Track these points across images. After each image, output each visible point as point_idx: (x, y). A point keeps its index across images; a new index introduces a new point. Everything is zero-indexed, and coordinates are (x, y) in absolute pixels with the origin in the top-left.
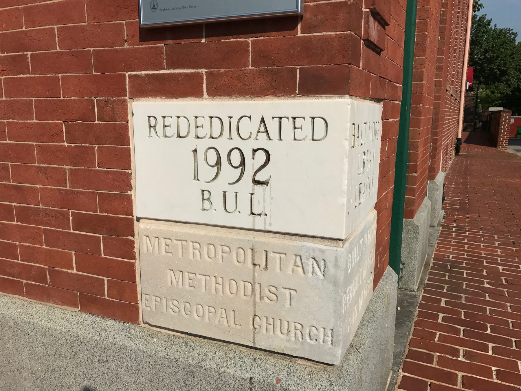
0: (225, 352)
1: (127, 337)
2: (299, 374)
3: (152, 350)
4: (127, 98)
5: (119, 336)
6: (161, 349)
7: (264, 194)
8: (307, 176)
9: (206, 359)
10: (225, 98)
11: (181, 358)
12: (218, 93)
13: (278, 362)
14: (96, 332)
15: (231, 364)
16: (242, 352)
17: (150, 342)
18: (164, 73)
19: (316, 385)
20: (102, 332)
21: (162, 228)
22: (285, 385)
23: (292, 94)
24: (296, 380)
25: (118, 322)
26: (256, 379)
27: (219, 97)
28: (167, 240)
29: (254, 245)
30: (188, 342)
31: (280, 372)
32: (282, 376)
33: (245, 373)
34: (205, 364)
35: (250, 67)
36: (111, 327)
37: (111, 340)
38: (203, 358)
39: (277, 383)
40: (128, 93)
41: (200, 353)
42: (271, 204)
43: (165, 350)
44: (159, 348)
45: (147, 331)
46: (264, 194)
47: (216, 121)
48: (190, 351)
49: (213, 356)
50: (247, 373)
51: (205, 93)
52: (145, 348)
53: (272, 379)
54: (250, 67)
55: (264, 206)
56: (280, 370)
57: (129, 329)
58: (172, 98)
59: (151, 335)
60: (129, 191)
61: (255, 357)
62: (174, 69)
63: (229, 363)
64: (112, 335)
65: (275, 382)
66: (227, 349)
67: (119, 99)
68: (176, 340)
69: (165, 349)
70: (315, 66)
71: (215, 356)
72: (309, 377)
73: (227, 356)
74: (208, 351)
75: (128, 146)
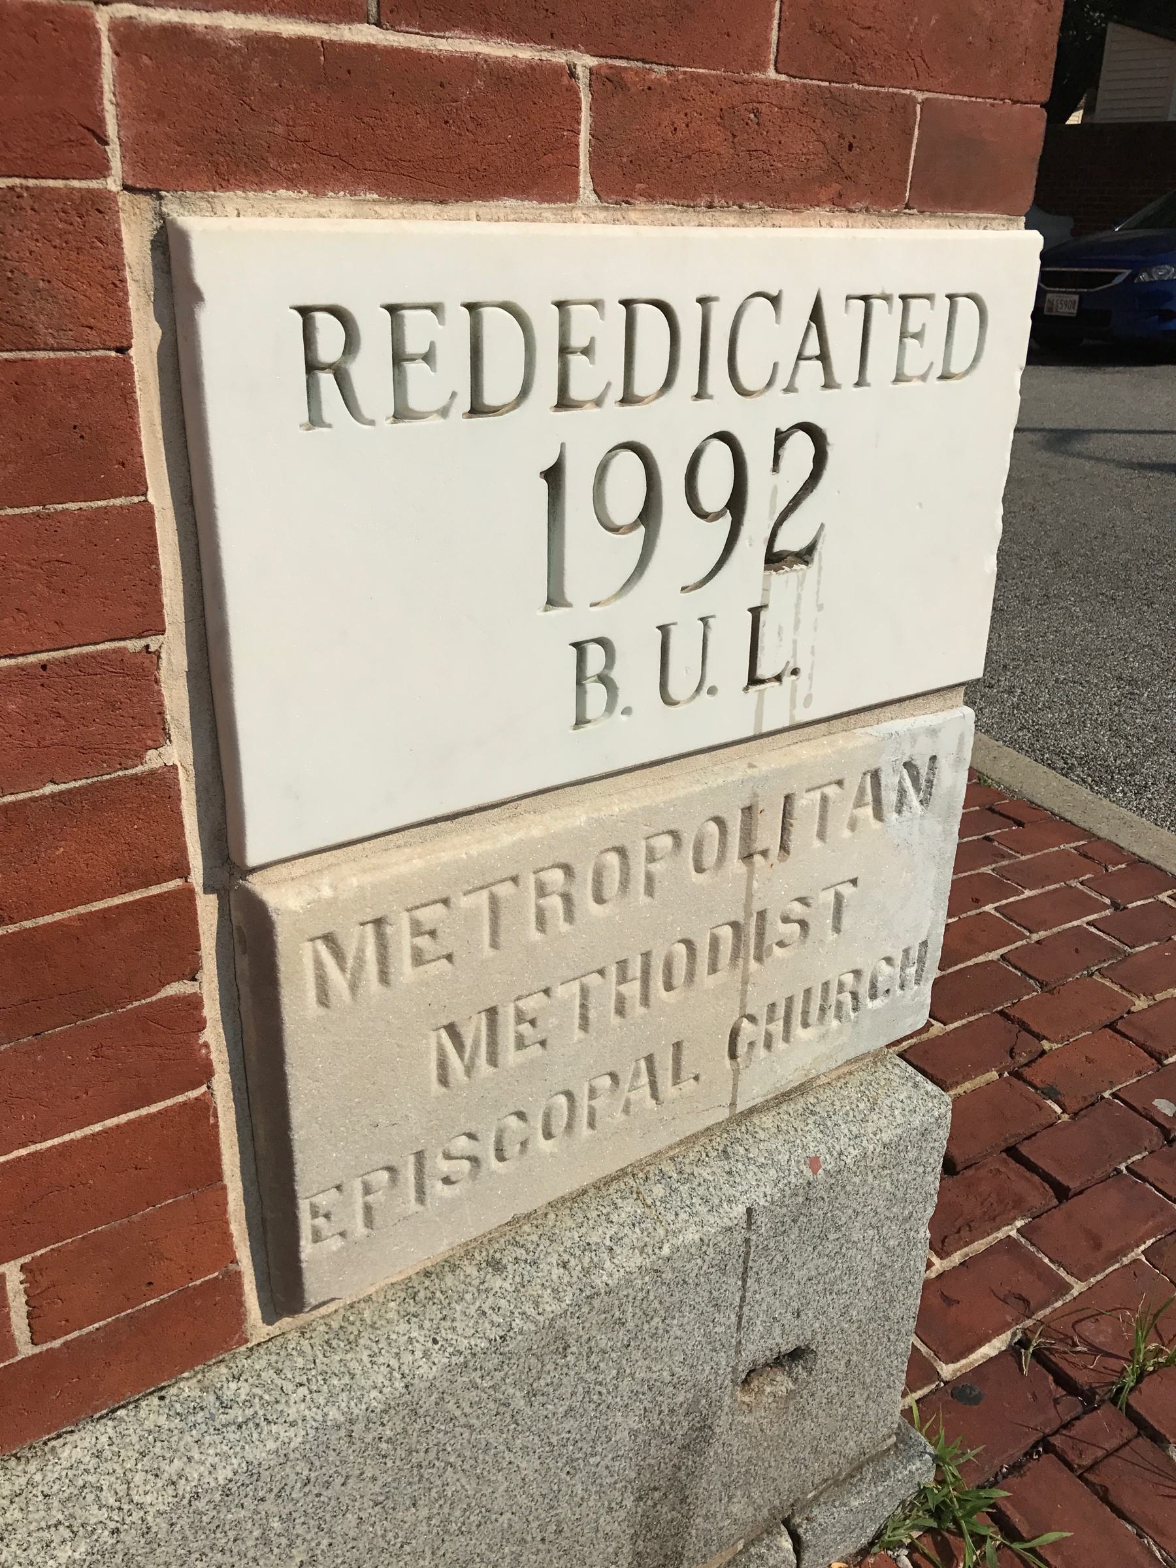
0: (635, 1196)
1: (233, 1428)
2: (844, 1110)
3: (387, 1383)
4: (113, 184)
5: (190, 1459)
6: (419, 1354)
7: (799, 597)
8: (920, 504)
9: (596, 1259)
10: (666, 211)
11: (514, 1324)
12: (642, 186)
13: (782, 1116)
14: (46, 1535)
15: (677, 1215)
16: (681, 1159)
17: (353, 1365)
18: (369, 46)
19: (891, 1108)
20: (78, 1512)
21: (404, 869)
22: (833, 1164)
23: (895, 205)
24: (846, 1131)
25: (121, 1413)
26: (762, 1202)
27: (643, 206)
28: (423, 910)
29: (758, 791)
30: (498, 1256)
31: (804, 1139)
32: (813, 1144)
33: (729, 1210)
34: (605, 1278)
35: (772, 74)
36: (107, 1454)
37: (156, 1499)
38: (586, 1265)
39: (815, 1172)
40: (114, 152)
41: (566, 1257)
42: (815, 629)
43: (437, 1347)
44: (407, 1358)
45: (303, 1341)
46: (799, 597)
47: (650, 321)
48: (526, 1278)
49: (610, 1233)
50: (733, 1205)
51: (585, 180)
52: (352, 1404)
53: (797, 1171)
54: (772, 74)
55: (795, 642)
56: (800, 1133)
57: (212, 1398)
58: (415, 200)
59: (334, 1343)
60: (151, 754)
61: (721, 1149)
62: (427, 29)
63: (670, 1217)
64: (146, 1482)
65: (808, 1173)
66: (632, 1182)
67: (44, 190)
68: (449, 1280)
69: (435, 1341)
70: (966, 99)
71: (615, 1229)
72: (866, 1099)
73: (649, 1201)
74: (583, 1230)
75: (136, 499)
